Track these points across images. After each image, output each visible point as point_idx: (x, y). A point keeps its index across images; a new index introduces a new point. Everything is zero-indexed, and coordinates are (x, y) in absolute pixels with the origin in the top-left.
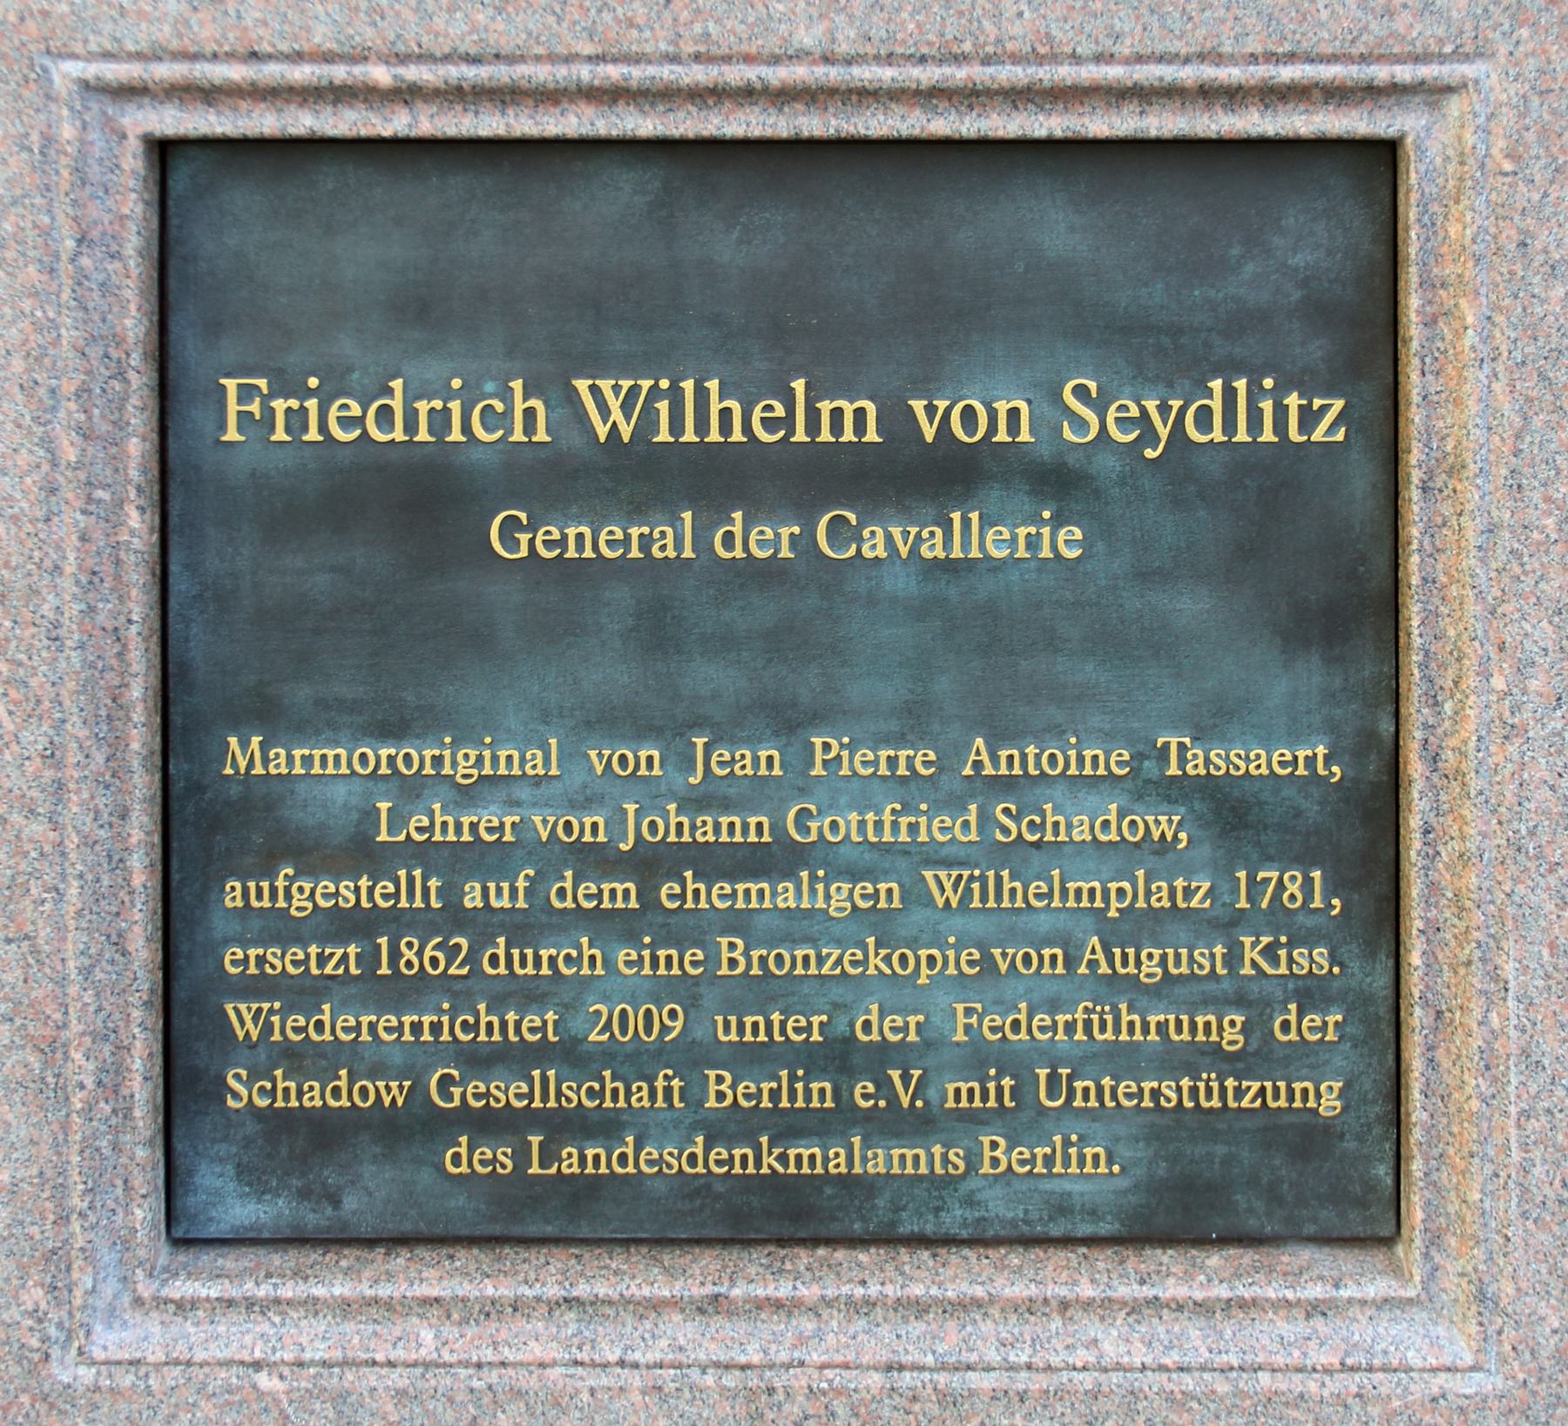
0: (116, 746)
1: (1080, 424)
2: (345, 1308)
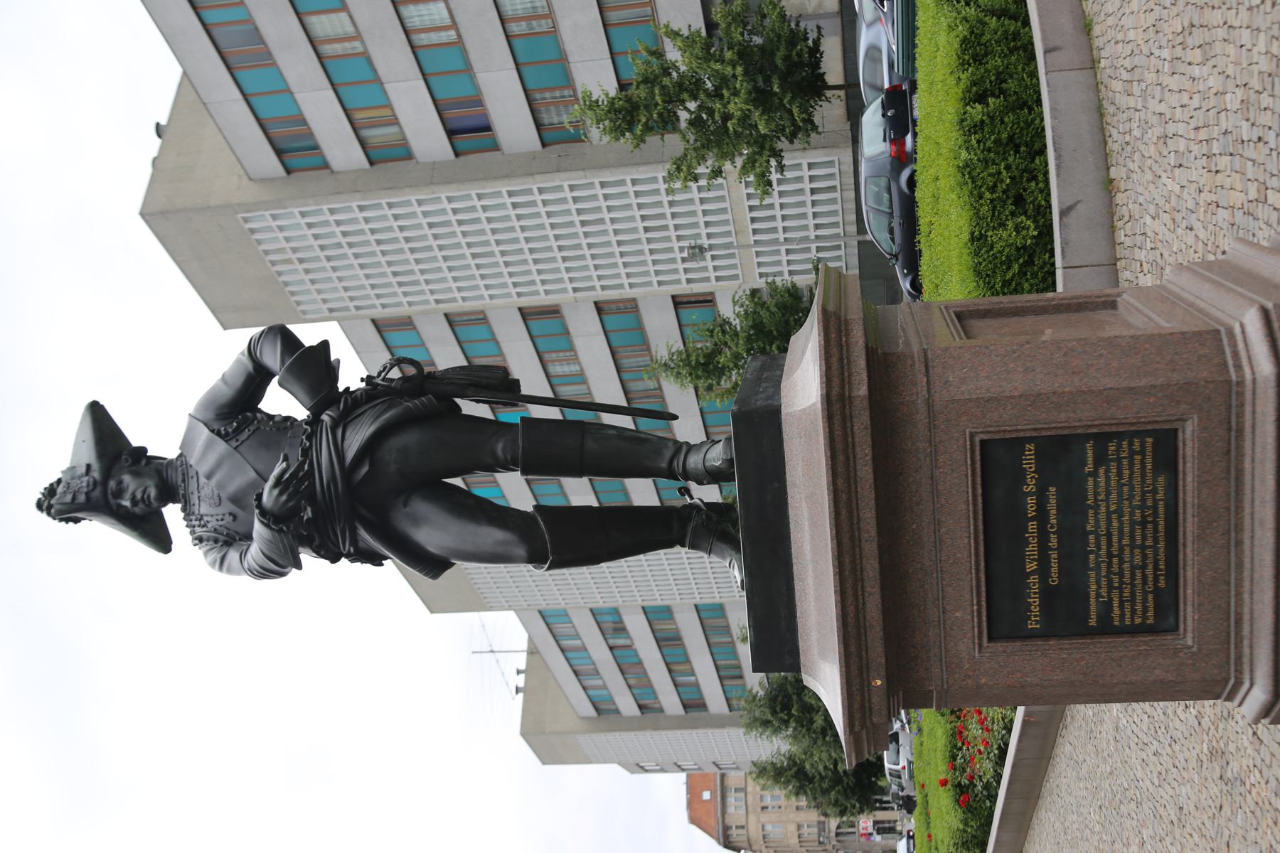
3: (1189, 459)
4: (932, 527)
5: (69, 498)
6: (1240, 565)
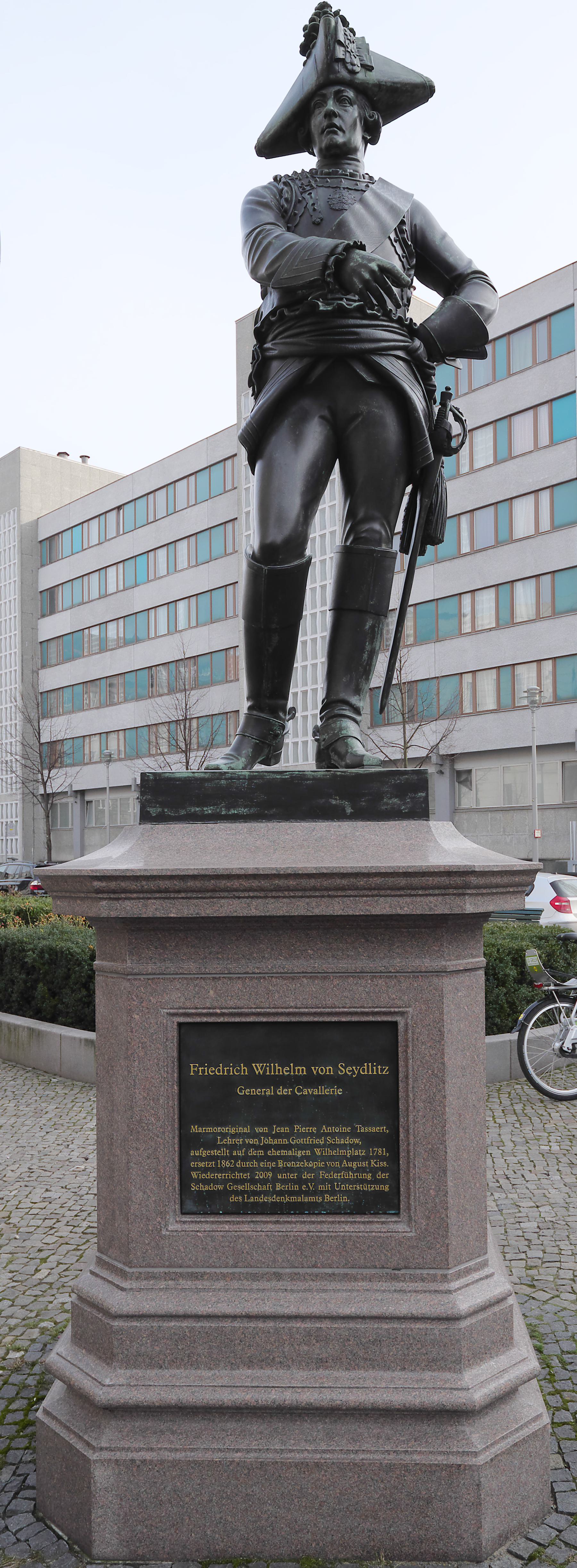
1: (342, 1071)
2: (213, 1222)
3: (368, 1228)
4: (309, 970)
5: (341, 38)
6: (255, 1277)
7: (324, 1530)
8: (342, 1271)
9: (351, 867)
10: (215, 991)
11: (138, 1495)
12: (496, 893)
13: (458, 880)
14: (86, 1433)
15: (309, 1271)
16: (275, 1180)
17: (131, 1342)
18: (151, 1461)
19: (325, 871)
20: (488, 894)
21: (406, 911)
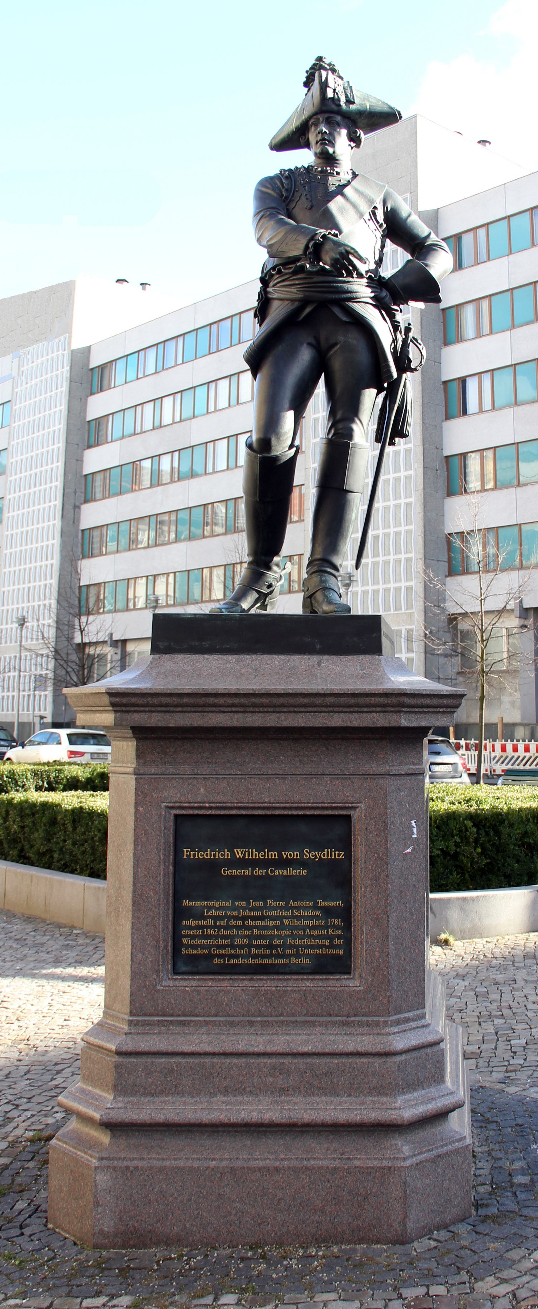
0: (168, 899)
1: (306, 856)
4: (281, 772)
6: (232, 1024)
7: (281, 1222)
8: (304, 1019)
9: (311, 689)
10: (205, 789)
11: (131, 1195)
12: (428, 712)
13: (394, 700)
14: (90, 1149)
15: (276, 1019)
16: (250, 946)
17: (129, 1074)
18: (142, 1167)
19: (291, 692)
20: (421, 712)
21: (355, 724)
